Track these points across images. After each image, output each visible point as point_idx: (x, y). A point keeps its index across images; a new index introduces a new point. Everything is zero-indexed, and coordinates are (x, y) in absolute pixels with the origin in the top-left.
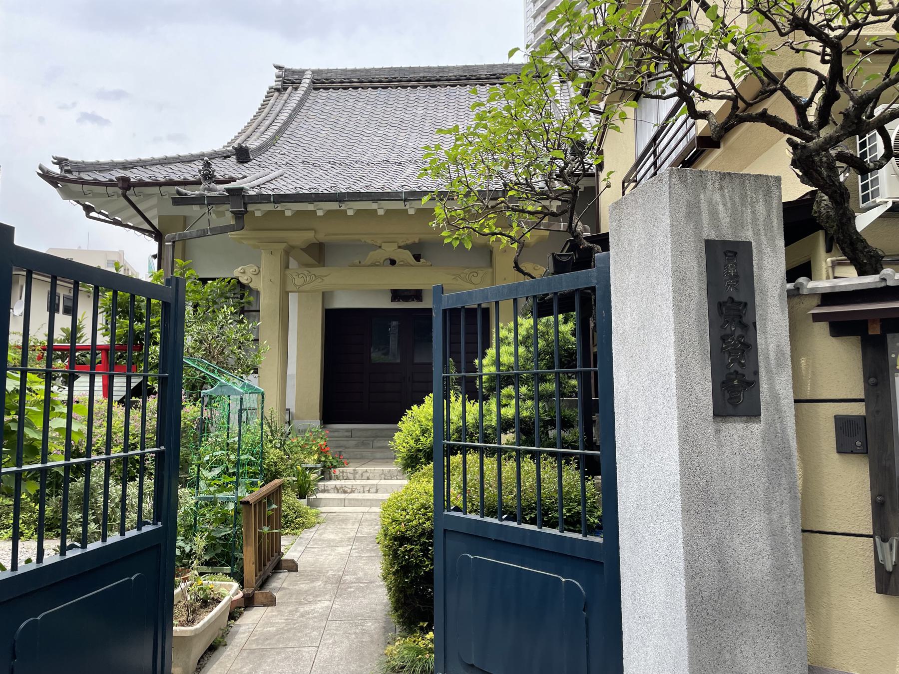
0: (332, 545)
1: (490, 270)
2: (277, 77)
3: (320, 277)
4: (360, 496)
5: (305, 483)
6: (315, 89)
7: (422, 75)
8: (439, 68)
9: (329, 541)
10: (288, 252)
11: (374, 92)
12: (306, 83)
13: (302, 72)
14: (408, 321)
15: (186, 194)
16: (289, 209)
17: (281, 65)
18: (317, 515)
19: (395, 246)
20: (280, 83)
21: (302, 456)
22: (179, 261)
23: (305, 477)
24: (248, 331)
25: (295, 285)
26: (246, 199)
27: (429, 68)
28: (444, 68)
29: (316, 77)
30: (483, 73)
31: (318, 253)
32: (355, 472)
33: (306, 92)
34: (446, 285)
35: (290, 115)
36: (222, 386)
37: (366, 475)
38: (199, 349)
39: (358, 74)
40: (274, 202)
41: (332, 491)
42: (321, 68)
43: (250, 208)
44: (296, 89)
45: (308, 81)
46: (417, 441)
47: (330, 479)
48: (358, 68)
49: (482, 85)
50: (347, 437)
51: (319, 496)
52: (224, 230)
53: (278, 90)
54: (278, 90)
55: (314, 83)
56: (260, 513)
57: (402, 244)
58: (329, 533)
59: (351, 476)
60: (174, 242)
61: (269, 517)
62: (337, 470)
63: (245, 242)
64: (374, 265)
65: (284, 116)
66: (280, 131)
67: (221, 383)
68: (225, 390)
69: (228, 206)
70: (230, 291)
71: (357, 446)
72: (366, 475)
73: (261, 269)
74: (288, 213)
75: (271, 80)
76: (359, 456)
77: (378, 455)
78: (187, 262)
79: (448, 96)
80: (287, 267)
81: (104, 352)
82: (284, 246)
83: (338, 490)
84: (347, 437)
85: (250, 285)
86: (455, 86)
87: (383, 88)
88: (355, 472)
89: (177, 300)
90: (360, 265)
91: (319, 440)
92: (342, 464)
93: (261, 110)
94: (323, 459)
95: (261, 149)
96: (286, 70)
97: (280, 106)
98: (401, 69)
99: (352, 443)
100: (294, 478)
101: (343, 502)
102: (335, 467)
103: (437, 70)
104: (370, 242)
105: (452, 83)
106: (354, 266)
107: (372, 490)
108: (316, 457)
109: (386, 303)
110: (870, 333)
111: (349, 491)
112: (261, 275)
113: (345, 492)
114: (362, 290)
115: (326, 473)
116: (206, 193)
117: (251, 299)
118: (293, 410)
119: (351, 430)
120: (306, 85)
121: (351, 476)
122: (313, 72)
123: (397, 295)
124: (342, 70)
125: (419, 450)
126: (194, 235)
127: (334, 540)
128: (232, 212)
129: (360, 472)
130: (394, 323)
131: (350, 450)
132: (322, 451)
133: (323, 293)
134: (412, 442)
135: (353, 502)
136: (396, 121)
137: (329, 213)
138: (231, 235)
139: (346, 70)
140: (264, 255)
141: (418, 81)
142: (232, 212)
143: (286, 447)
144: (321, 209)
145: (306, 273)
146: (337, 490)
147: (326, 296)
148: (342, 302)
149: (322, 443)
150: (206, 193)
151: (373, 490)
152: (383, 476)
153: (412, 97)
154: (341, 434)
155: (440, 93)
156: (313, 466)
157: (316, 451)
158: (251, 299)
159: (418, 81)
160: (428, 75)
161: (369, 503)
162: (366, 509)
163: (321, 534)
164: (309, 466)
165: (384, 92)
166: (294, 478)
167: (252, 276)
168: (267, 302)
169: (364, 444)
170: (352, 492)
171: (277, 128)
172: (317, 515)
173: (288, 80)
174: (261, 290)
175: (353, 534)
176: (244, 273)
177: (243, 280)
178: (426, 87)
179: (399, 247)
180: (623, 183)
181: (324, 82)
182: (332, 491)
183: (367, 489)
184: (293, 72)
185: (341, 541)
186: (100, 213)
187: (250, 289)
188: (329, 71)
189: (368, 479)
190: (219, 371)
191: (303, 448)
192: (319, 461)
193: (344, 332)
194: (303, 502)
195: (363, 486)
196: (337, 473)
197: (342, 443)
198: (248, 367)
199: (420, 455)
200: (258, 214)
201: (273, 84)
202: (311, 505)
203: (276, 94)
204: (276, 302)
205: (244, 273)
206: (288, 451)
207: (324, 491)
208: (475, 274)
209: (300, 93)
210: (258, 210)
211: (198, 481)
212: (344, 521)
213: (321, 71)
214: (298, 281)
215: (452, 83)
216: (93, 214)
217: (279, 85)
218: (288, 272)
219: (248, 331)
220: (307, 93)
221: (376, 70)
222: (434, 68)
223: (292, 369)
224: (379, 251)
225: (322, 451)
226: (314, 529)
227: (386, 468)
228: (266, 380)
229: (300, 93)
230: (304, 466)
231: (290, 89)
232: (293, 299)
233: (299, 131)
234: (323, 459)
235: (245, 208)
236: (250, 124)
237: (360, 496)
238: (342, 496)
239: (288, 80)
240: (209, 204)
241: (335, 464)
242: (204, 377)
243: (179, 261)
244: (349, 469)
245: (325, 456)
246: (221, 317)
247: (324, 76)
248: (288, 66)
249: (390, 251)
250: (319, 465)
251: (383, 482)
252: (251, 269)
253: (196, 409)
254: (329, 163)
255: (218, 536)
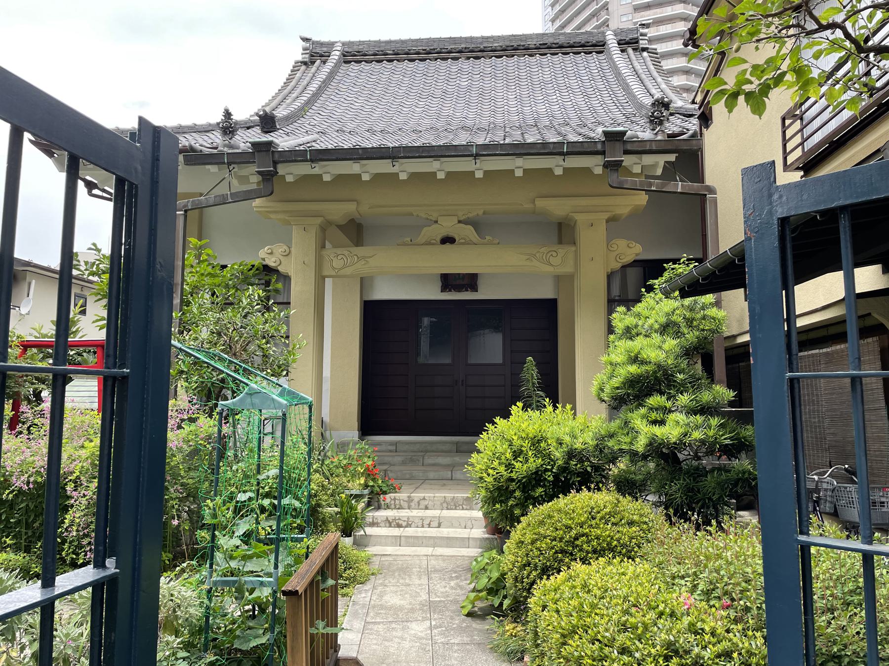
0: (401, 617)
1: (573, 248)
2: (305, 49)
3: (364, 258)
4: (420, 532)
5: (351, 517)
6: (345, 62)
7: (463, 46)
8: (483, 38)
9: (396, 610)
10: (324, 229)
11: (411, 65)
12: (336, 55)
13: (331, 44)
14: (461, 312)
15: (201, 151)
16: (329, 171)
17: (308, 37)
18: (368, 561)
19: (455, 220)
20: (307, 56)
21: (345, 480)
22: (193, 240)
23: (351, 508)
24: (279, 321)
25: (334, 268)
26: (276, 156)
27: (471, 38)
28: (488, 38)
29: (346, 50)
30: (532, 43)
31: (356, 232)
32: (410, 500)
33: (336, 64)
34: (509, 272)
35: (320, 87)
36: (252, 394)
37: (423, 503)
38: (216, 344)
39: (393, 46)
40: (312, 161)
41: (382, 524)
42: (352, 40)
43: (282, 169)
44: (324, 62)
45: (338, 53)
46: (509, 466)
47: (379, 508)
48: (393, 39)
49: (531, 55)
50: (391, 451)
51: (369, 531)
52: (248, 196)
53: (305, 63)
54: (305, 63)
55: (344, 56)
56: (311, 599)
57: (462, 219)
58: (393, 596)
59: (405, 505)
60: (186, 211)
61: (323, 601)
62: (387, 496)
63: (273, 216)
64: (429, 243)
65: (314, 87)
66: (310, 102)
67: (251, 389)
68: (256, 400)
69: (254, 168)
70: (254, 275)
71: (404, 463)
72: (423, 503)
73: (293, 249)
74: (327, 178)
75: (297, 53)
76: (408, 476)
77: (431, 475)
78: (203, 242)
79: (494, 67)
80: (323, 246)
81: (99, 351)
82: (319, 220)
83: (390, 523)
84: (391, 451)
85: (279, 268)
86: (501, 57)
87: (420, 60)
88: (410, 500)
89: (154, 183)
90: (412, 244)
91: (366, 459)
92: (394, 489)
93: (286, 84)
94: (371, 483)
95: (290, 119)
96: (313, 43)
97: (308, 79)
98: (440, 40)
99: (398, 459)
100: (336, 509)
101: (398, 541)
102: (385, 493)
103: (481, 40)
104: (423, 215)
105: (497, 53)
106: (405, 244)
107: (433, 524)
108: (362, 481)
109: (433, 293)
110: (499, 360)
111: (404, 524)
112: (293, 258)
113: (399, 526)
114: (406, 276)
115: (374, 500)
116: (226, 149)
117: (280, 286)
118: (327, 419)
119: (396, 444)
120: (337, 58)
121: (405, 505)
122: (344, 44)
123: (448, 281)
124: (375, 42)
125: (511, 480)
126: (211, 202)
127: (401, 608)
128: (259, 173)
129: (416, 500)
130: (426, 321)
131: (396, 468)
132: (369, 473)
133: (362, 279)
134: (502, 469)
135: (411, 540)
136: (438, 93)
137: (378, 178)
138: (258, 202)
139: (379, 42)
140: (296, 234)
141: (460, 52)
142: (259, 173)
143: (325, 468)
144: (368, 169)
145: (346, 253)
146: (389, 523)
147: (365, 283)
148: (384, 292)
149: (370, 463)
150: (226, 149)
151: (435, 524)
152: (445, 505)
153: (454, 69)
154: (384, 448)
155: (485, 64)
156: (358, 492)
157: (362, 474)
158: (280, 286)
159: (460, 52)
160: (471, 46)
161: (432, 542)
162: (429, 551)
163: (381, 596)
164: (354, 492)
165: (421, 65)
166: (336, 509)
167: (281, 258)
168: (300, 289)
169: (412, 461)
170: (409, 526)
171: (305, 99)
172: (368, 561)
173: (316, 53)
174: (292, 273)
175: (424, 597)
176: (271, 253)
177: (271, 262)
178: (468, 58)
179: (460, 222)
180: (784, 120)
181: (356, 54)
182: (382, 524)
183: (426, 522)
184: (322, 44)
185: (412, 610)
186: (104, 191)
187: (276, 271)
188: (361, 43)
189: (426, 508)
190: (245, 370)
191: (345, 468)
192: (366, 486)
193: (382, 325)
194: (348, 541)
195: (422, 519)
196: (388, 501)
197: (387, 459)
198: (279, 367)
199: (513, 486)
200: (289, 179)
201: (300, 58)
202: (357, 544)
203: (303, 67)
204: (310, 288)
205: (271, 253)
206: (328, 474)
207: (373, 524)
208: (554, 254)
209: (330, 64)
210: (289, 172)
211: (213, 552)
212: (405, 570)
213: (353, 43)
214: (337, 263)
215: (497, 53)
216: (96, 192)
217: (307, 58)
218: (324, 252)
219: (279, 321)
220: (337, 66)
221: (413, 41)
222: (477, 38)
223: (327, 373)
224: (435, 226)
225: (369, 473)
226: (368, 586)
227: (449, 495)
228: (300, 381)
229: (330, 64)
230: (347, 492)
231: (318, 62)
232: (329, 282)
233: (330, 103)
234: (371, 483)
235: (275, 168)
236: (274, 98)
237: (420, 532)
238: (396, 532)
239: (316, 53)
240: (229, 164)
241: (384, 489)
242: (223, 381)
243: (193, 240)
244: (402, 496)
245: (374, 480)
246: (245, 302)
247: (356, 48)
248: (315, 38)
249: (449, 226)
250: (366, 492)
251: (446, 513)
252: (280, 249)
253: (212, 422)
254: (368, 131)
255: (244, 647)
